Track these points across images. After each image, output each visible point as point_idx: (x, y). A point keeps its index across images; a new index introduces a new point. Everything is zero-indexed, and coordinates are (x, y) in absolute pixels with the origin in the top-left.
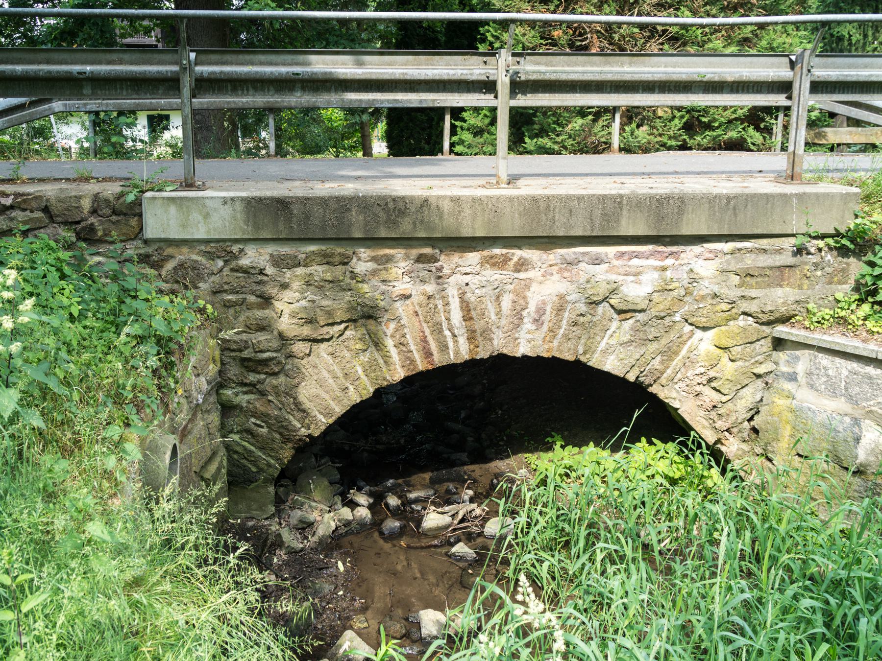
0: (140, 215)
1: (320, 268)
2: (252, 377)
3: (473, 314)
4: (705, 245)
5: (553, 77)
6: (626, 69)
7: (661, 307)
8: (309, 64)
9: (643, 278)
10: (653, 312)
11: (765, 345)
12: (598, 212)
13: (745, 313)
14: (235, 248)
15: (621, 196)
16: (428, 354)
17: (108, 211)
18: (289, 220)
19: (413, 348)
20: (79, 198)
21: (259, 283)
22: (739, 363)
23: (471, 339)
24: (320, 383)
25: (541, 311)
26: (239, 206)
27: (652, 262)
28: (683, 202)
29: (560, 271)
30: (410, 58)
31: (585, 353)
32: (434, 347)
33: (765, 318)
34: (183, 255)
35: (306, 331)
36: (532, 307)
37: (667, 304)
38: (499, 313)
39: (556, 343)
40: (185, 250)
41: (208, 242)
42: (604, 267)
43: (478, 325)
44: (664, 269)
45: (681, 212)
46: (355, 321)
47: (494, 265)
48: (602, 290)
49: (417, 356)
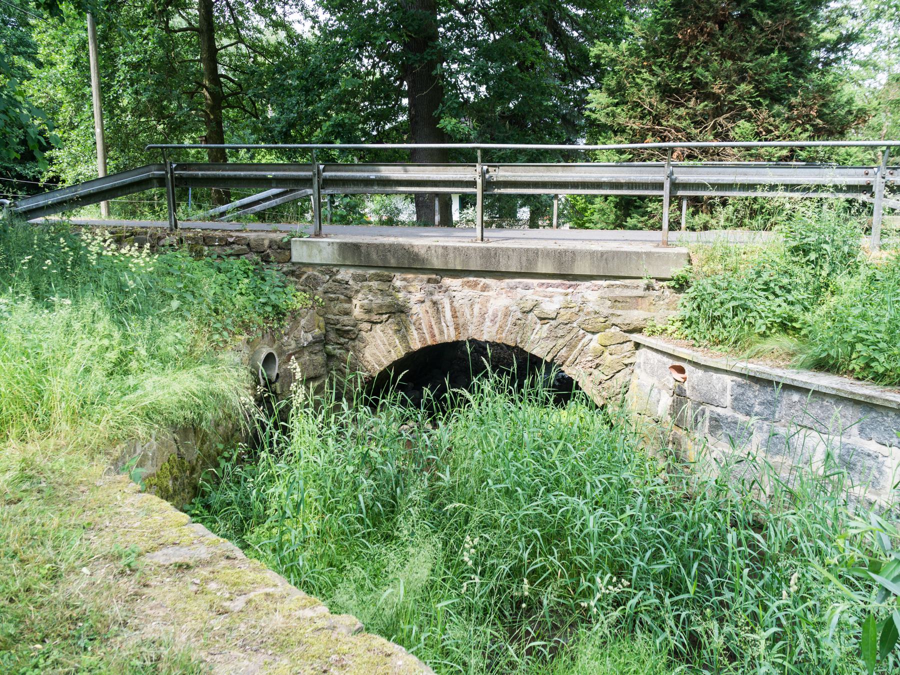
0: (290, 249)
1: (376, 283)
2: (342, 340)
3: (458, 314)
4: (593, 282)
5: (513, 179)
6: (560, 174)
7: (565, 317)
8: (379, 171)
9: (555, 299)
10: (559, 320)
11: (629, 346)
12: (524, 258)
13: (613, 325)
14: (335, 270)
15: (538, 250)
16: (433, 336)
17: (276, 247)
18: (360, 255)
19: (425, 331)
20: (263, 239)
21: (346, 289)
22: (614, 356)
23: (456, 329)
24: (376, 346)
25: (495, 316)
26: (336, 247)
27: (560, 290)
28: (574, 254)
29: (506, 292)
30: (434, 168)
31: (521, 342)
32: (436, 332)
33: (625, 328)
34: (310, 272)
35: (366, 317)
36: (490, 313)
37: (568, 316)
38: (472, 315)
39: (504, 335)
40: (311, 269)
41: (322, 265)
42: (531, 291)
43: (461, 321)
44: (567, 295)
45: (573, 260)
46: (394, 313)
47: (469, 286)
48: (529, 305)
49: (428, 336)
